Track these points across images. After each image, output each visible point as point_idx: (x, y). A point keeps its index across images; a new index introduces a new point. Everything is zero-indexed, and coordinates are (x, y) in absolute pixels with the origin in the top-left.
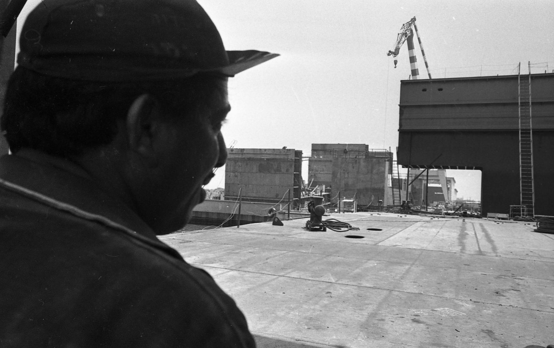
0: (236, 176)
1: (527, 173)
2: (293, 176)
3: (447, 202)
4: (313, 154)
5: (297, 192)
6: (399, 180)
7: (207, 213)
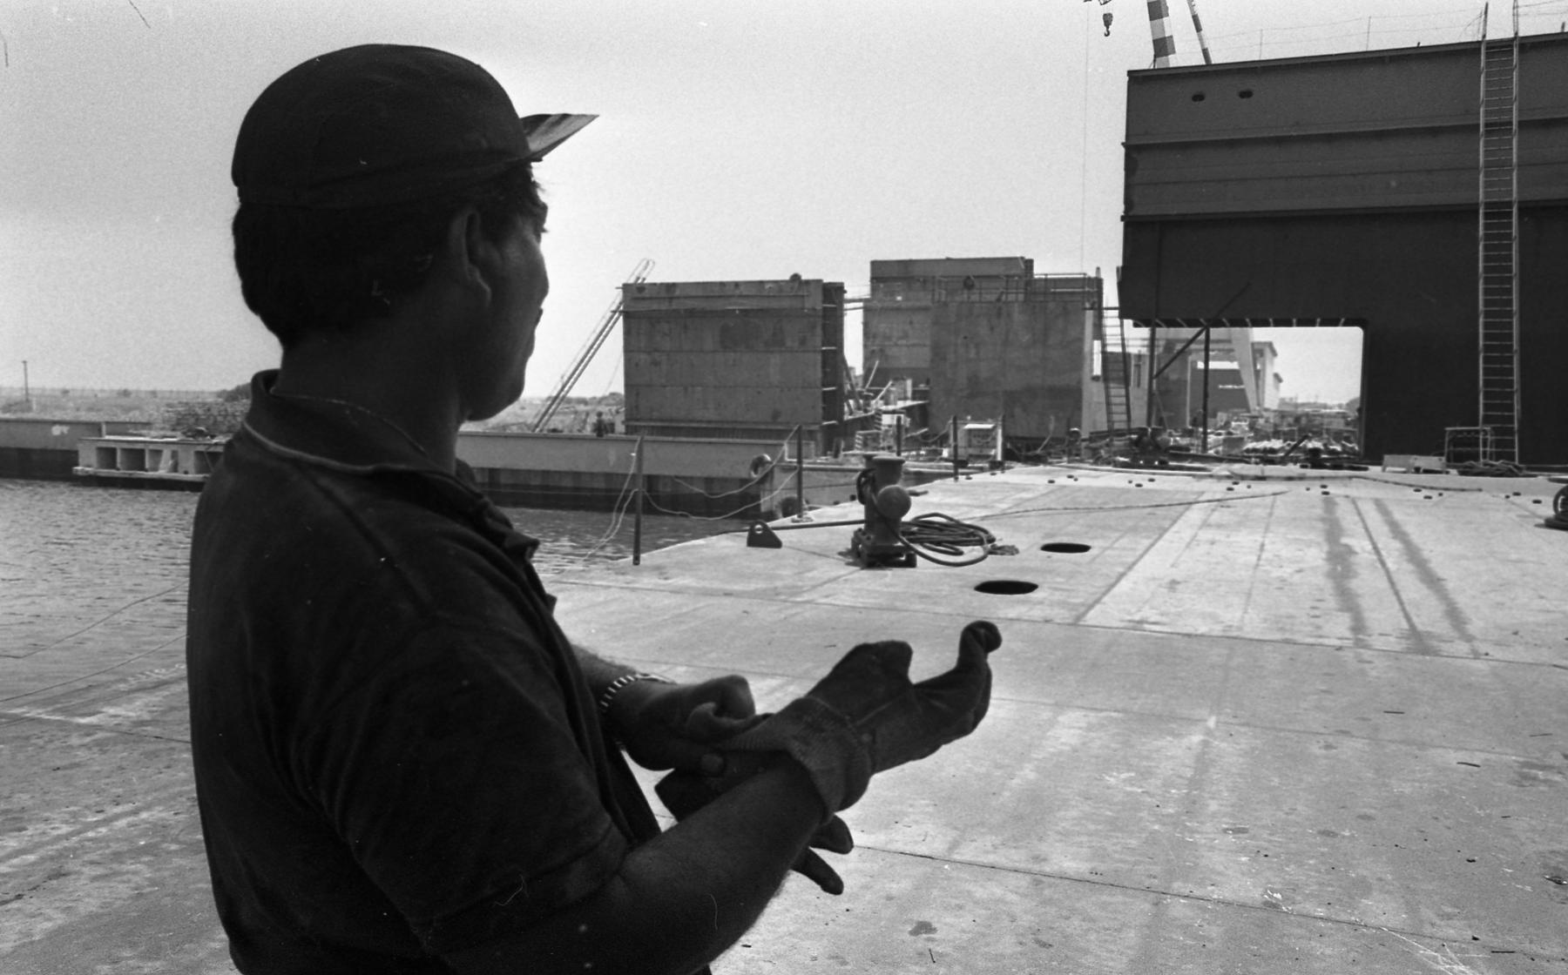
0: (656, 363)
1: (1498, 335)
2: (819, 357)
3: (1254, 414)
4: (874, 289)
5: (833, 403)
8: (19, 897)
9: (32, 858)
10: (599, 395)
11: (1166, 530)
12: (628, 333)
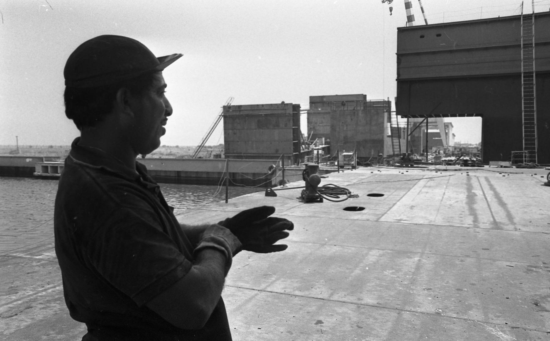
0: (235, 134)
1: (529, 119)
2: (292, 131)
3: (445, 148)
4: (311, 106)
5: (297, 146)
6: (398, 129)
7: (208, 173)
8: (16, 315)
9: (20, 302)
10: (215, 145)
11: (411, 189)
12: (225, 123)
